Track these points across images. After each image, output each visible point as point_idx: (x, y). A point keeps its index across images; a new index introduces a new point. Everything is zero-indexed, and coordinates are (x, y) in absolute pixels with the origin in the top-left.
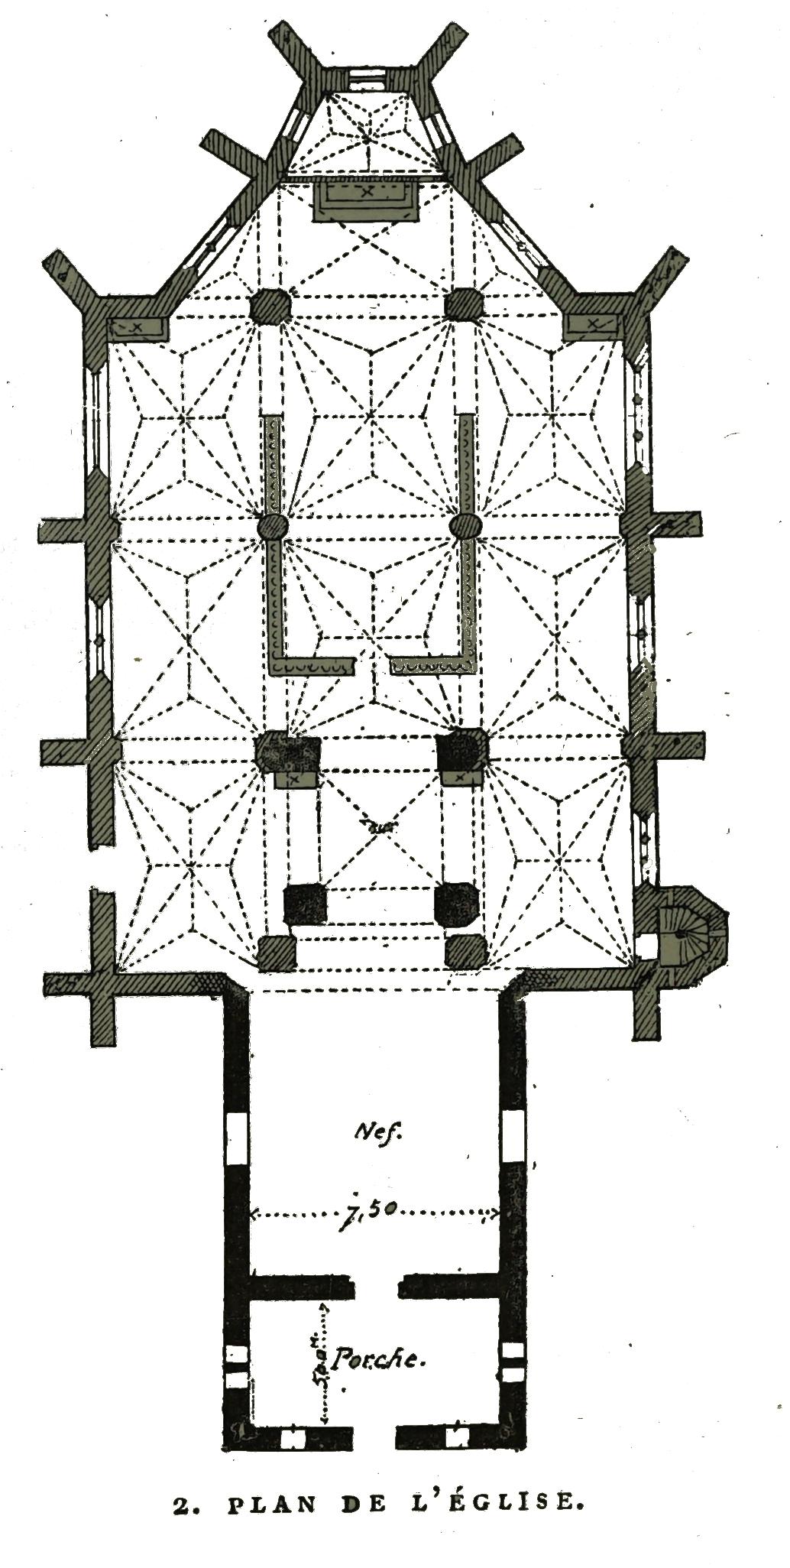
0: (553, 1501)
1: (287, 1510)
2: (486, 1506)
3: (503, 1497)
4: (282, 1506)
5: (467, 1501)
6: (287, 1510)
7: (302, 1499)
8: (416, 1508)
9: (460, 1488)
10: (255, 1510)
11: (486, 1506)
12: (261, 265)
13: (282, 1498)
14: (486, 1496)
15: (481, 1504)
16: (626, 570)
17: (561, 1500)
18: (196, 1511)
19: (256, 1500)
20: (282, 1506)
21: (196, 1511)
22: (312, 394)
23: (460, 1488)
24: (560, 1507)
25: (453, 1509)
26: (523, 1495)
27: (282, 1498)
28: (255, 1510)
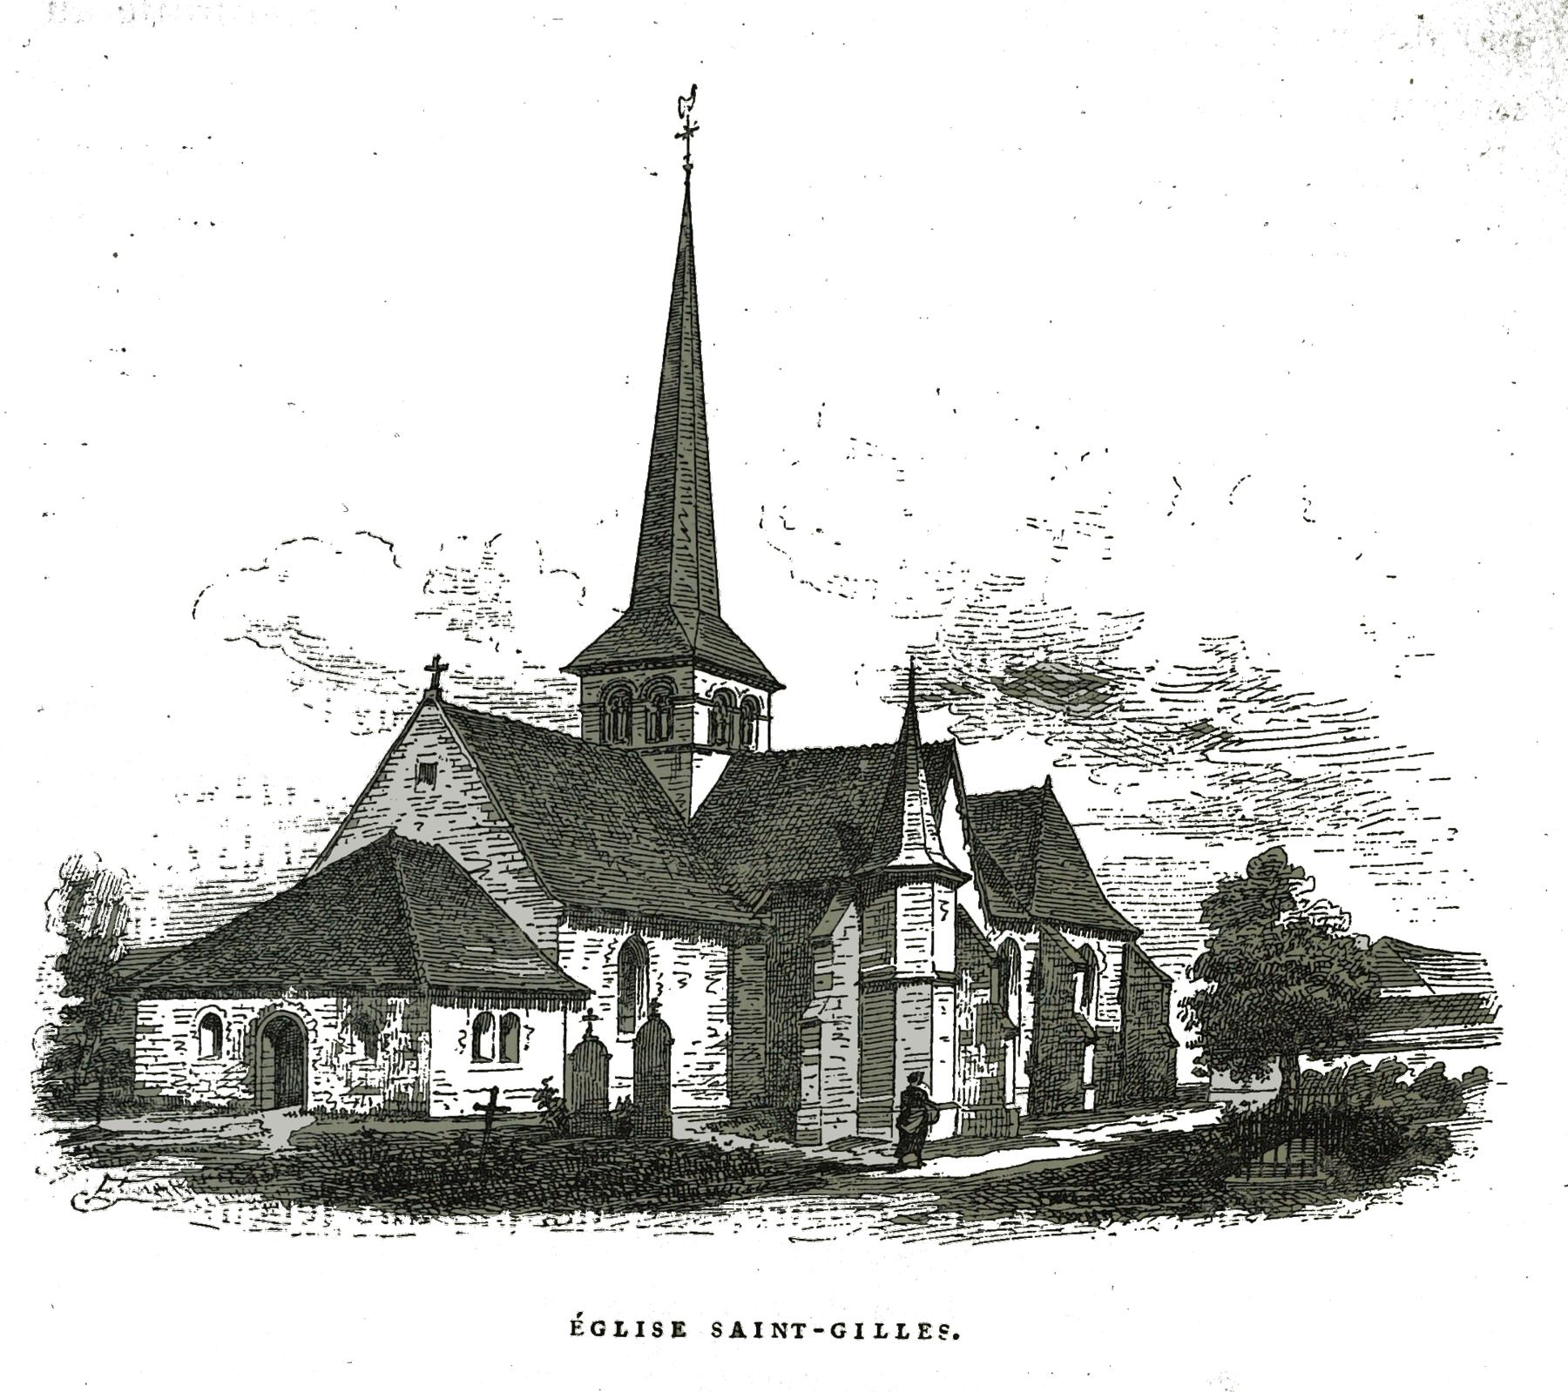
0: (668, 1329)
1: (742, 1335)
2: (603, 1332)
3: (901, 1326)
4: (738, 1332)
5: (586, 1327)
6: (742, 1335)
7: (775, 1325)
8: (878, 1336)
9: (580, 1314)
10: (618, 1334)
11: (843, 1333)
12: (299, 537)
13: (738, 1324)
14: (602, 1323)
15: (598, 1329)
16: (876, 746)
17: (574, 1327)
18: (956, 1337)
19: (619, 1324)
20: (738, 1332)
21: (956, 1337)
22: (759, 515)
23: (580, 1314)
24: (921, 1337)
25: (573, 1333)
26: (758, 1325)
27: (738, 1324)
28: (618, 1334)
